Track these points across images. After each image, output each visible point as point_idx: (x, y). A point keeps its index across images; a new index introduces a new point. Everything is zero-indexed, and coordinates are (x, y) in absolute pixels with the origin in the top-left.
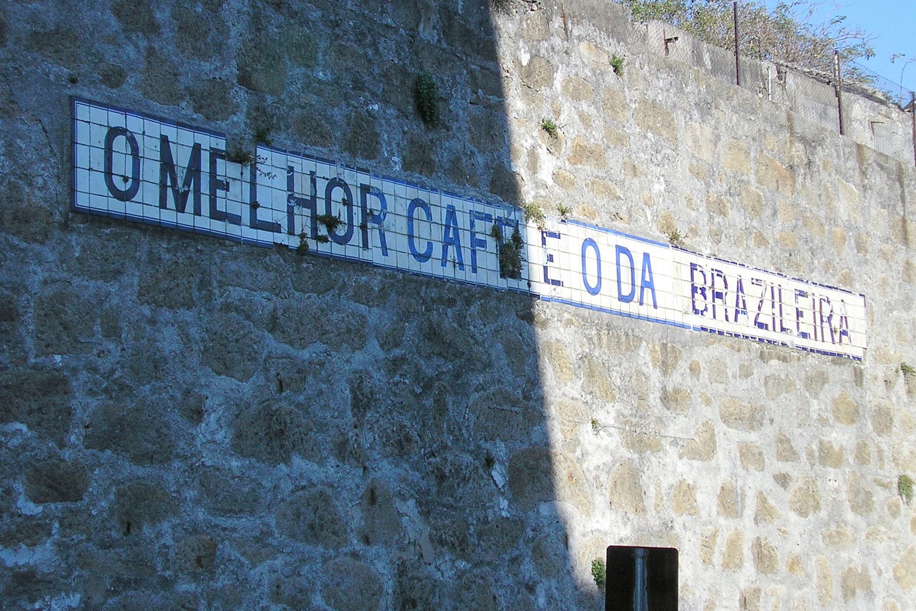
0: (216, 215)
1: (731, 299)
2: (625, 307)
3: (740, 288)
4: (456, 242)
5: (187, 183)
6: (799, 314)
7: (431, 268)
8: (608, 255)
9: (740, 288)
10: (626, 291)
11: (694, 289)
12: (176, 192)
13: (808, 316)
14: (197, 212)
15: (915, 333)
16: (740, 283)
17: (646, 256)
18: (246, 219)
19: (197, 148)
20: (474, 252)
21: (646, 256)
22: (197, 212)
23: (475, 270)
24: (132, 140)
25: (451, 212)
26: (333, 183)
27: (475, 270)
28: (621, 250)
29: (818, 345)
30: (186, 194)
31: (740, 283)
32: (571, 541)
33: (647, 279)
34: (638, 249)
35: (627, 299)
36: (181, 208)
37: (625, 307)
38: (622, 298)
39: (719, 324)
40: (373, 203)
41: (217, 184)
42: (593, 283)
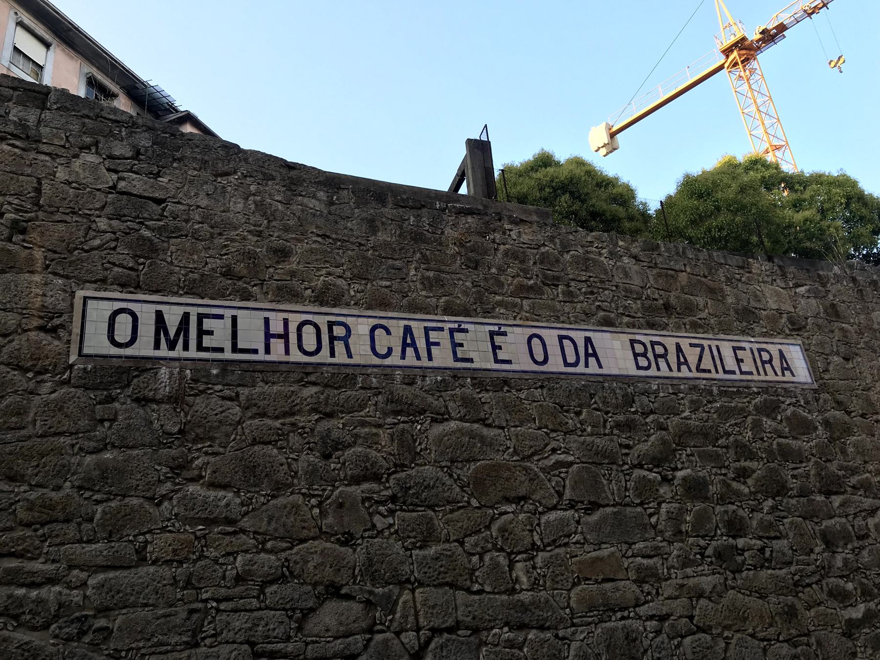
1: (776, 362)
5: (177, 334)
18: (738, 372)
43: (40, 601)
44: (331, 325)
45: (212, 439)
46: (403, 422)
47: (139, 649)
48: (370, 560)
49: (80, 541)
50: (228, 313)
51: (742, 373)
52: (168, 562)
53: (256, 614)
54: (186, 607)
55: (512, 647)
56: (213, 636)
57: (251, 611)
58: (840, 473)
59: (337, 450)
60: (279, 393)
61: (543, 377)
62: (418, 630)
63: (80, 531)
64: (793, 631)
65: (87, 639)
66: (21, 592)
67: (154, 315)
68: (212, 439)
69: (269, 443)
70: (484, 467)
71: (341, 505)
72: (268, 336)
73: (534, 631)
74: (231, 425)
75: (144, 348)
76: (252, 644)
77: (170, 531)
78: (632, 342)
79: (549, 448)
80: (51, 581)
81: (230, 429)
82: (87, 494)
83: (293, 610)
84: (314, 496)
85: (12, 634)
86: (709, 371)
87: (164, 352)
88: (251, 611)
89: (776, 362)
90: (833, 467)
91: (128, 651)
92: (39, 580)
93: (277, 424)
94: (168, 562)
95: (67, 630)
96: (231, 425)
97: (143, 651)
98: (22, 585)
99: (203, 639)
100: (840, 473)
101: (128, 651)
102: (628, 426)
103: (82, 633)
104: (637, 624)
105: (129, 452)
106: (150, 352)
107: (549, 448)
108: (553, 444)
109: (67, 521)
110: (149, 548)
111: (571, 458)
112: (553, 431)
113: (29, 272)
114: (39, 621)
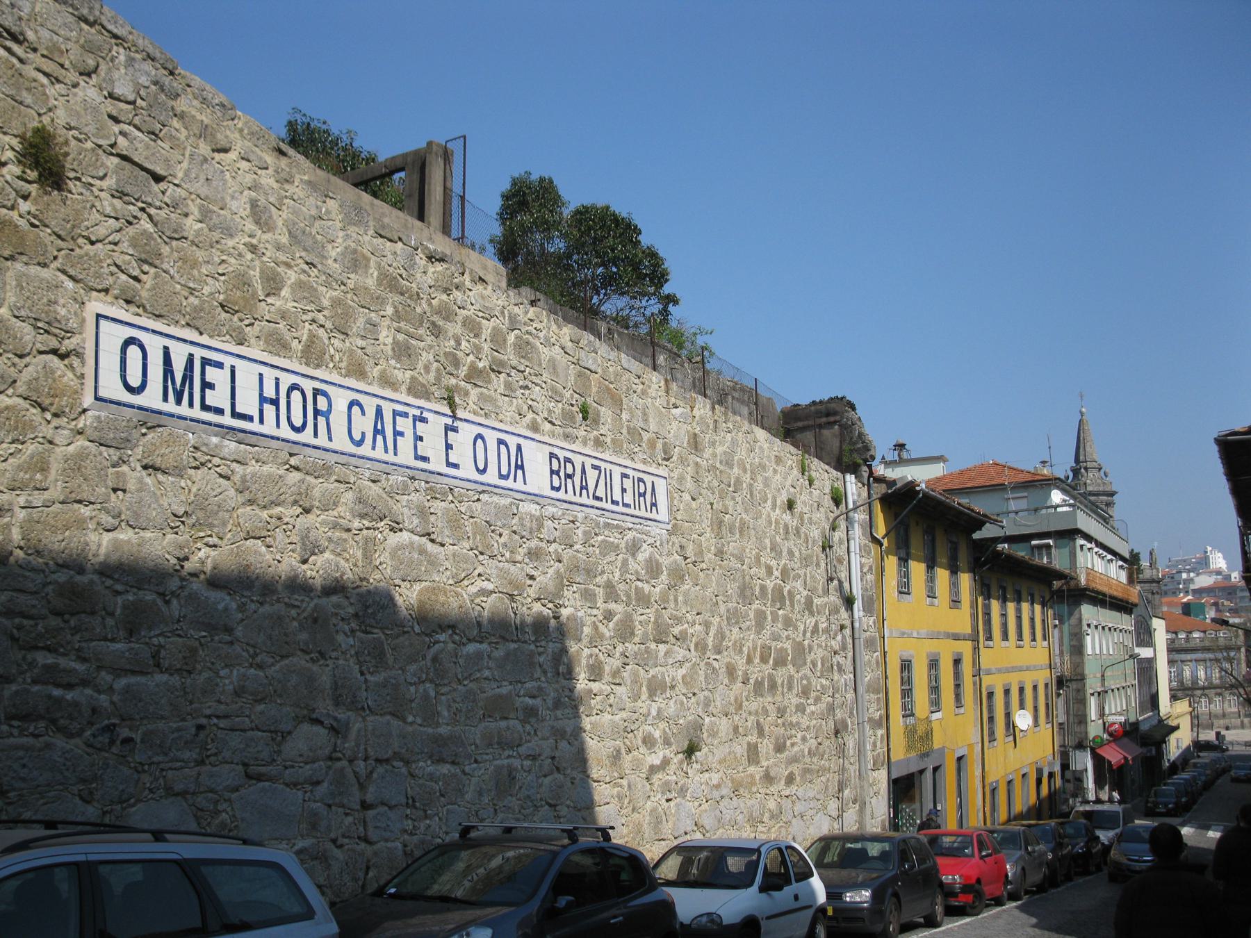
0: (205, 407)
1: (577, 478)
2: (503, 483)
3: (583, 471)
4: (382, 432)
5: (183, 384)
6: (624, 490)
7: (365, 450)
8: (492, 446)
9: (583, 471)
10: (298, 422)
11: (552, 472)
12: (175, 389)
13: (630, 491)
14: (191, 405)
15: (1250, 696)
16: (583, 466)
17: (519, 447)
18: (228, 411)
19: (191, 358)
20: (395, 441)
21: (519, 447)
22: (191, 405)
23: (396, 454)
24: (142, 347)
25: (379, 412)
26: (294, 387)
27: (396, 454)
28: (501, 442)
29: (637, 513)
30: (182, 392)
31: (583, 466)
32: (970, 466)
33: (379, 427)
34: (513, 442)
35: (506, 477)
36: (179, 402)
37: (503, 483)
38: (502, 477)
39: (570, 496)
40: (322, 403)
41: (206, 385)
42: (481, 467)
43: (76, 704)
44: (316, 392)
45: (211, 526)
46: (368, 529)
47: (159, 763)
48: (336, 683)
49: (106, 639)
50: (228, 361)
51: (234, 414)
52: (178, 671)
53: (250, 733)
54: (194, 722)
55: (431, 780)
56: (216, 754)
57: (244, 731)
58: (670, 622)
59: (313, 554)
60: (270, 475)
61: (481, 488)
62: (365, 760)
63: (105, 627)
64: (616, 774)
65: (114, 750)
66: (57, 692)
67: (1215, 448)
68: (211, 526)
69: (259, 538)
70: (426, 589)
71: (315, 620)
72: (263, 399)
73: (448, 766)
74: (227, 511)
75: (152, 397)
76: (245, 765)
77: (179, 636)
78: (552, 455)
79: (476, 572)
80: (84, 683)
81: (227, 515)
82: (109, 582)
83: (276, 732)
84: (294, 606)
85: (53, 740)
86: (250, 419)
87: (170, 407)
88: (244, 731)
89: (577, 478)
90: (666, 614)
91: (150, 764)
92: (74, 680)
93: (265, 514)
94: (178, 671)
95: (100, 738)
96: (227, 511)
97: (162, 766)
98: (58, 685)
99: (208, 757)
100: (670, 622)
101: (150, 764)
102: (534, 555)
103: (112, 742)
104: (516, 763)
105: (142, 533)
106: (158, 404)
107: (476, 572)
108: (480, 569)
109: (93, 613)
110: (163, 653)
111: (490, 587)
112: (482, 553)
113: (39, 264)
114: (75, 726)
